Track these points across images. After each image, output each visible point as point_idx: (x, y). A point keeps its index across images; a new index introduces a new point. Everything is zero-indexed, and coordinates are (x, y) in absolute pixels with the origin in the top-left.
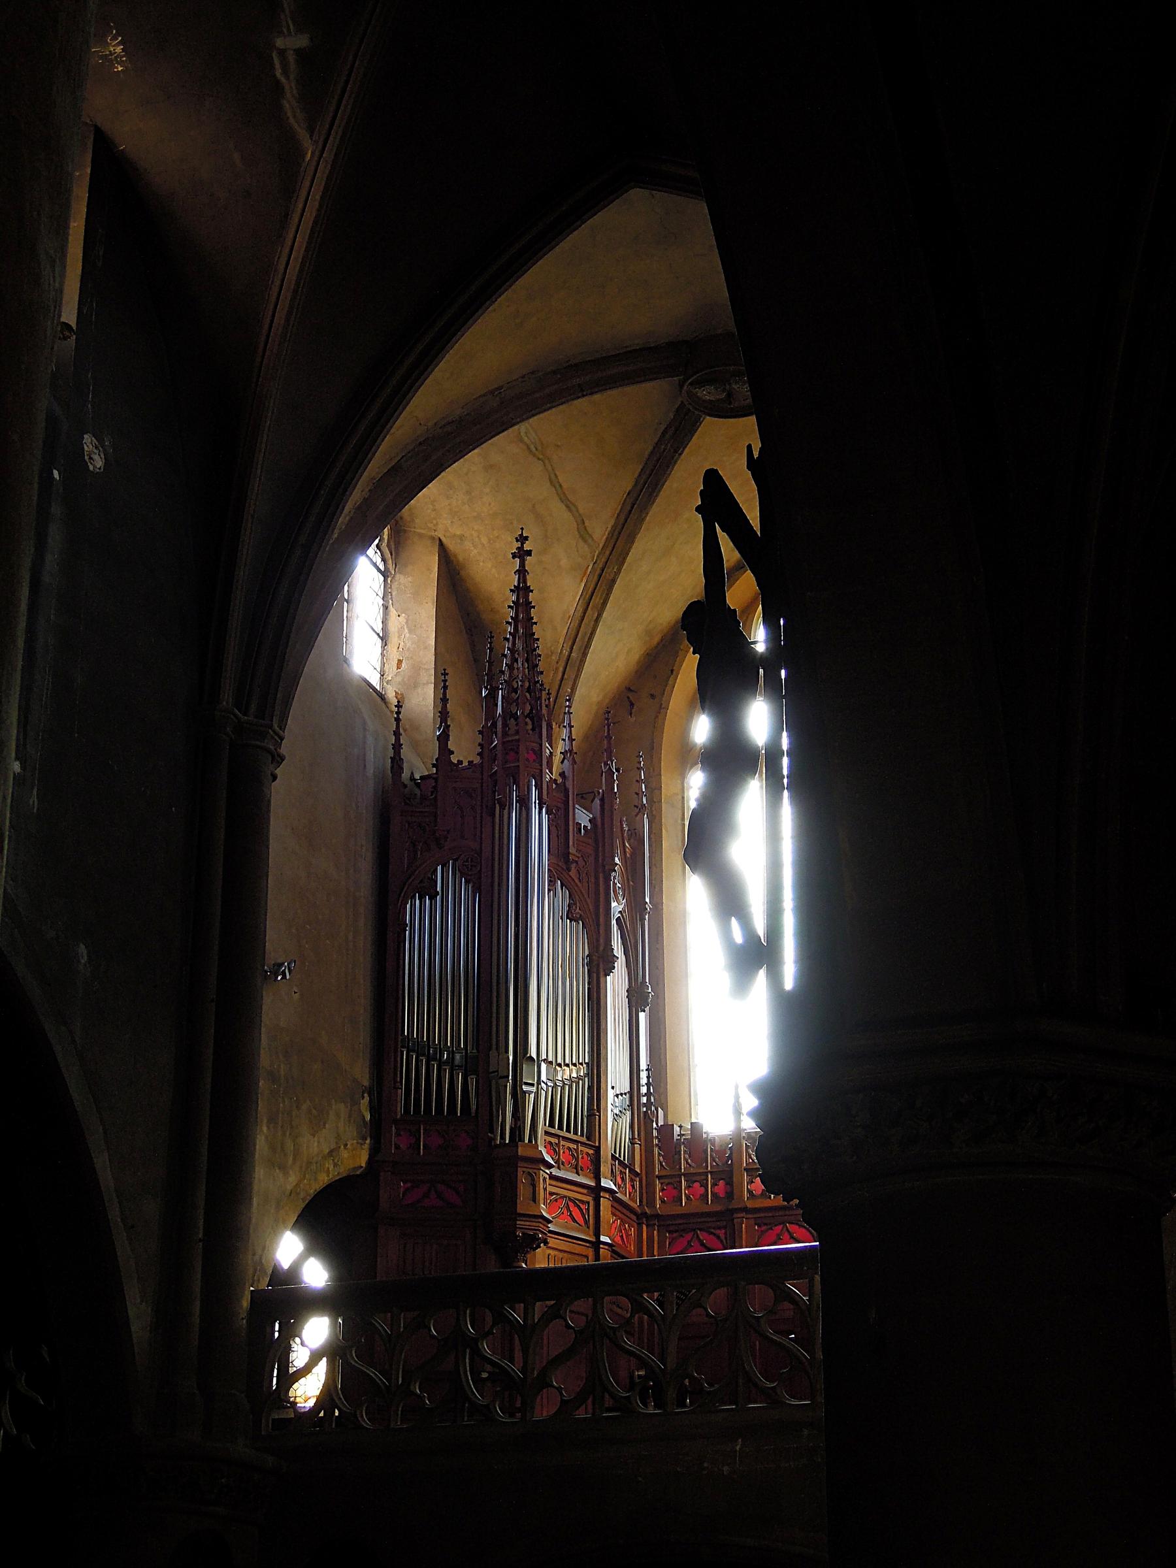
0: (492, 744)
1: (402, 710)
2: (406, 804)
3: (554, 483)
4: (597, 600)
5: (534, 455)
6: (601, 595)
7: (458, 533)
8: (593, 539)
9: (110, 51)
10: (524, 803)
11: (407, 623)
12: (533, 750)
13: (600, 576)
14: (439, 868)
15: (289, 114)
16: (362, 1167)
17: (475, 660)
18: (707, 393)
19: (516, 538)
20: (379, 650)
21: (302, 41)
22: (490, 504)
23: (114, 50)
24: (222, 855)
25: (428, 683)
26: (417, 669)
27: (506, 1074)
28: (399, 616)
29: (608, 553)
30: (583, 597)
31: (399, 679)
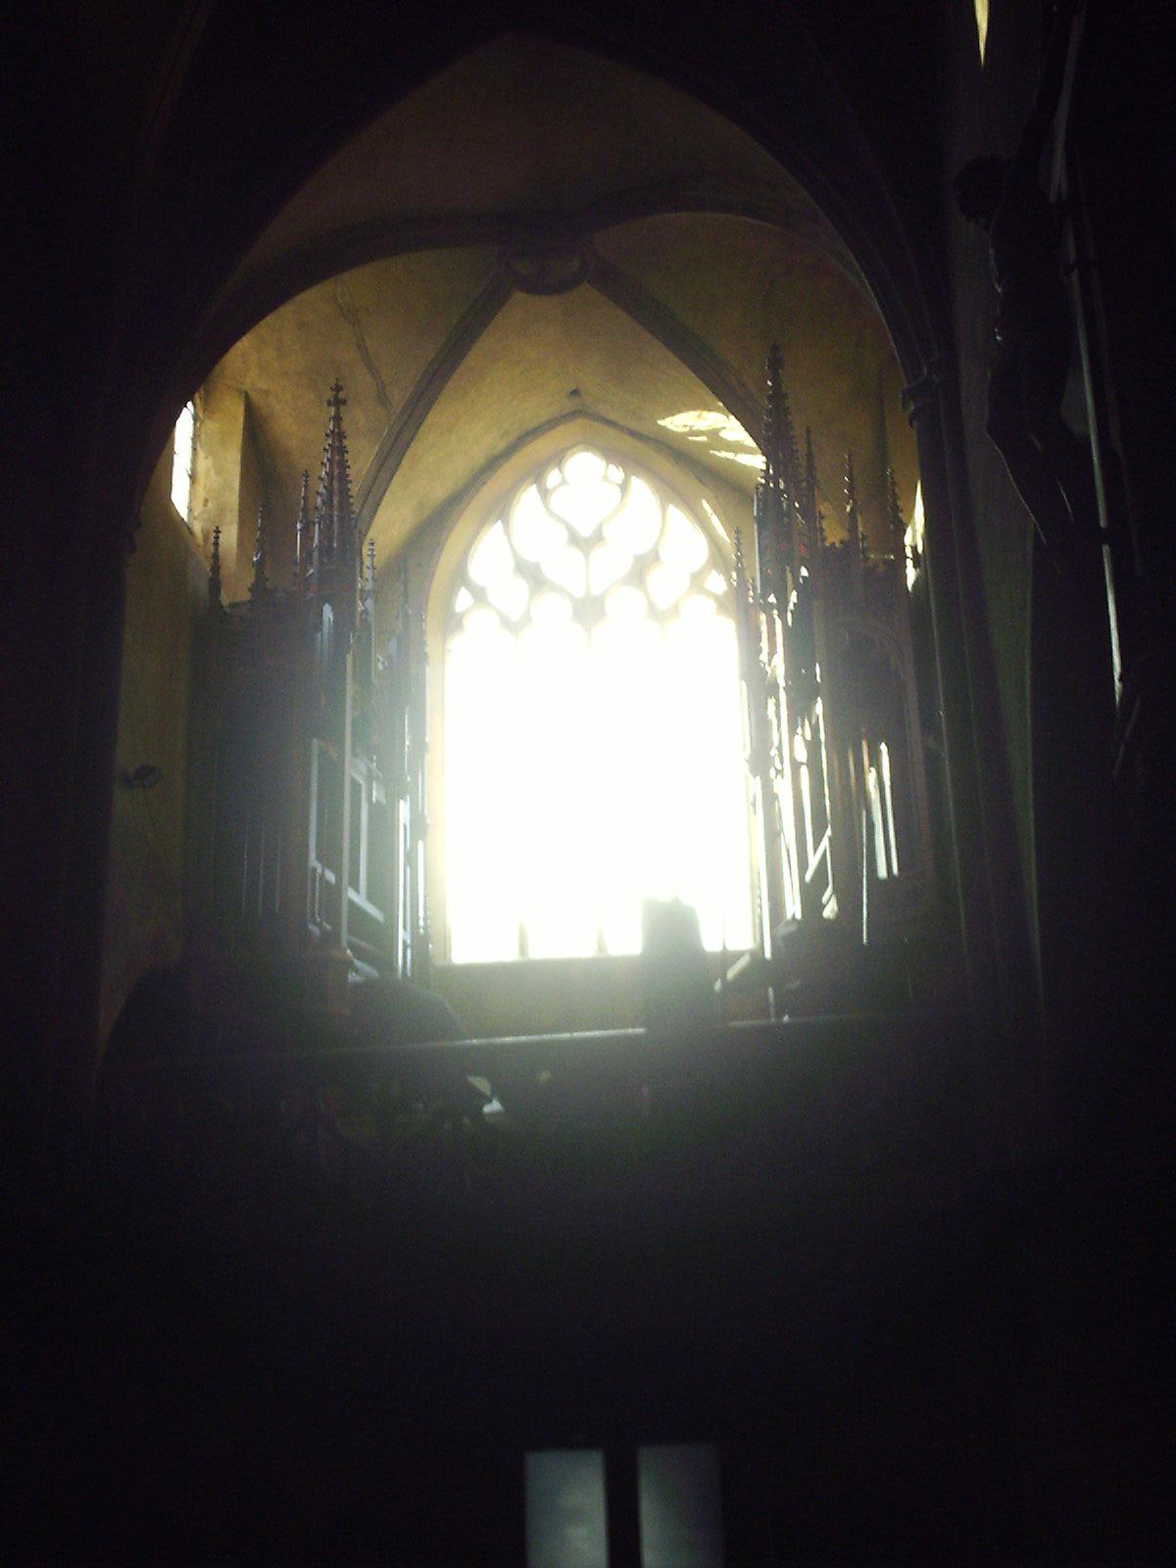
1: (220, 535)
3: (361, 347)
20: (188, 488)
24: (742, 218)
25: (232, 523)
26: (222, 509)
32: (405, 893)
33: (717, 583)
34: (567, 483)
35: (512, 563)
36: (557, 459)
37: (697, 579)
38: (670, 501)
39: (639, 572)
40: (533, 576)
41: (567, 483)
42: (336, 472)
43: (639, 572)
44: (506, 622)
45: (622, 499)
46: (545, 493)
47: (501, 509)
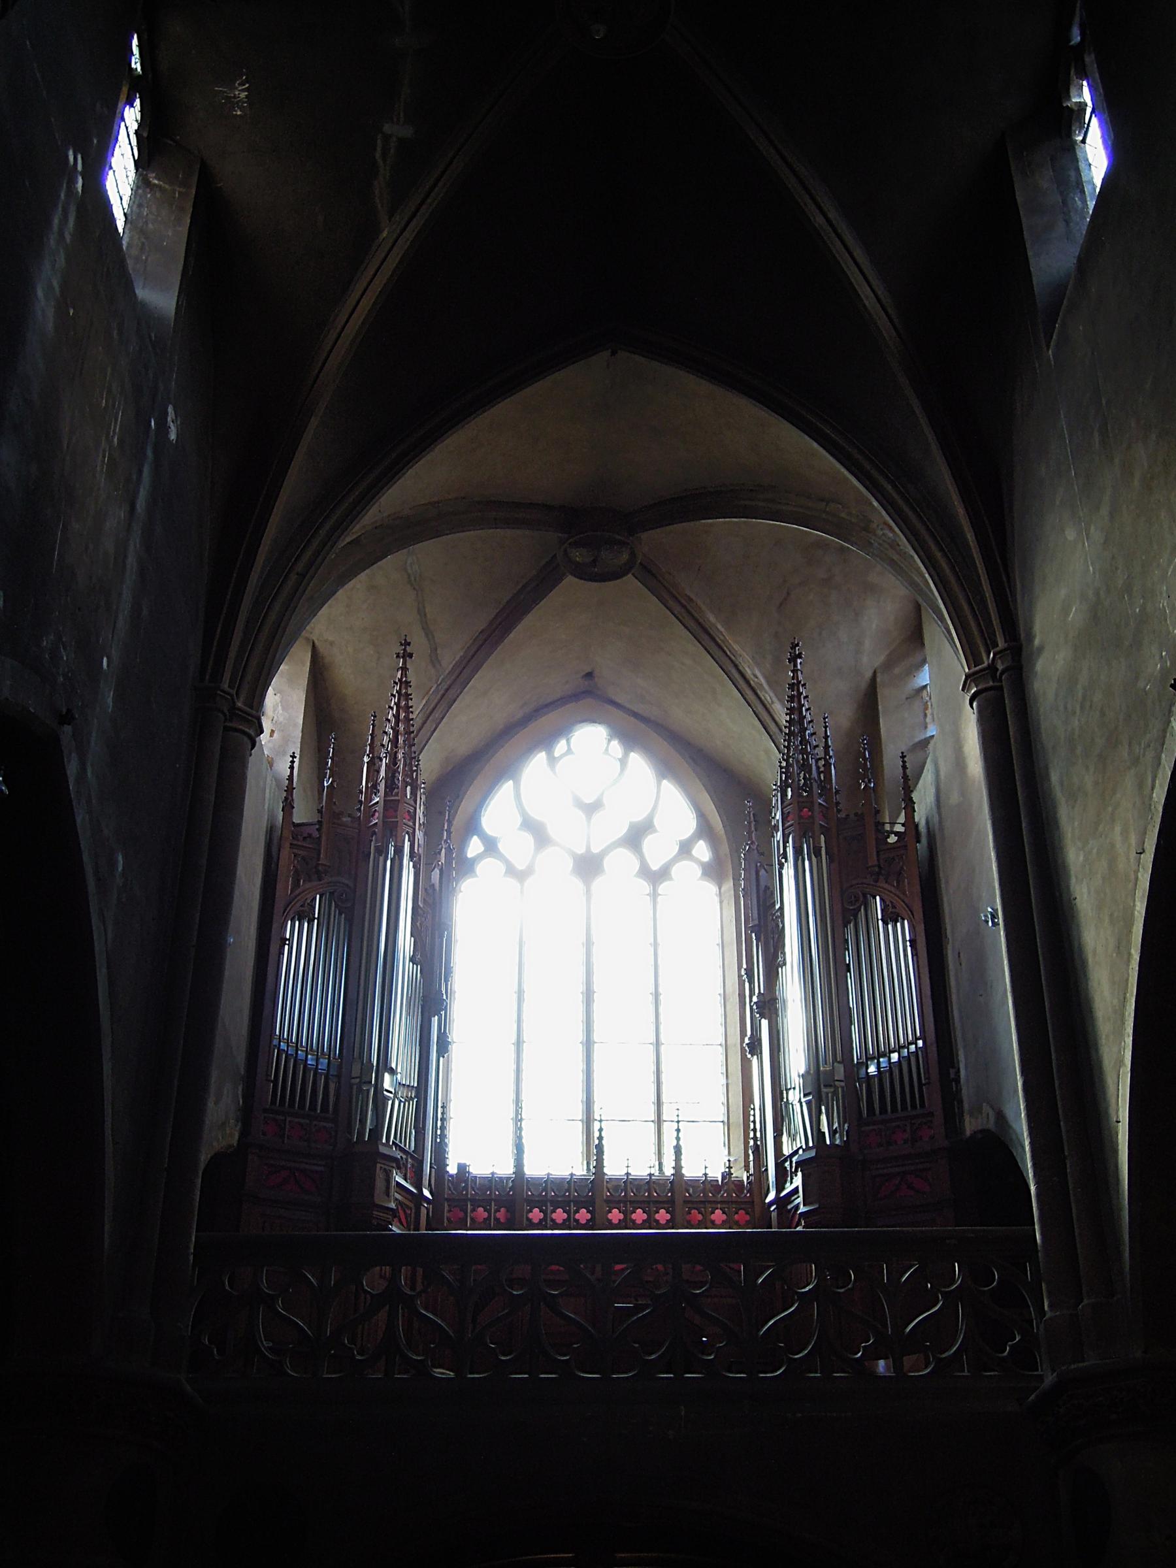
0: (371, 802)
2: (293, 838)
3: (422, 613)
4: (437, 714)
5: (412, 585)
6: (442, 712)
7: (331, 639)
8: (441, 665)
9: (235, 95)
10: (399, 851)
11: (281, 702)
12: (409, 812)
13: (443, 695)
14: (318, 896)
15: (377, 192)
16: (234, 1146)
17: (319, 750)
18: (578, 555)
19: (401, 643)
21: (407, 132)
22: (363, 619)
23: (239, 94)
27: (368, 1080)
28: (275, 694)
29: (453, 677)
30: (423, 711)
31: (270, 745)
32: (412, 1115)
33: (703, 851)
34: (572, 753)
35: (519, 820)
36: (562, 730)
37: (685, 849)
38: (664, 777)
39: (635, 837)
40: (537, 832)
41: (572, 753)
42: (402, 715)
43: (635, 837)
44: (511, 871)
45: (620, 775)
46: (552, 760)
47: (508, 770)
